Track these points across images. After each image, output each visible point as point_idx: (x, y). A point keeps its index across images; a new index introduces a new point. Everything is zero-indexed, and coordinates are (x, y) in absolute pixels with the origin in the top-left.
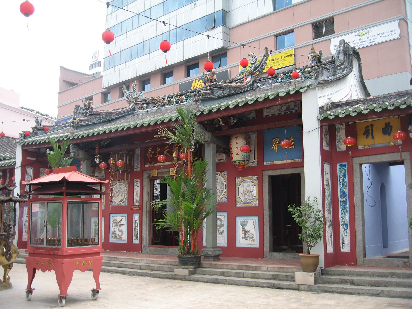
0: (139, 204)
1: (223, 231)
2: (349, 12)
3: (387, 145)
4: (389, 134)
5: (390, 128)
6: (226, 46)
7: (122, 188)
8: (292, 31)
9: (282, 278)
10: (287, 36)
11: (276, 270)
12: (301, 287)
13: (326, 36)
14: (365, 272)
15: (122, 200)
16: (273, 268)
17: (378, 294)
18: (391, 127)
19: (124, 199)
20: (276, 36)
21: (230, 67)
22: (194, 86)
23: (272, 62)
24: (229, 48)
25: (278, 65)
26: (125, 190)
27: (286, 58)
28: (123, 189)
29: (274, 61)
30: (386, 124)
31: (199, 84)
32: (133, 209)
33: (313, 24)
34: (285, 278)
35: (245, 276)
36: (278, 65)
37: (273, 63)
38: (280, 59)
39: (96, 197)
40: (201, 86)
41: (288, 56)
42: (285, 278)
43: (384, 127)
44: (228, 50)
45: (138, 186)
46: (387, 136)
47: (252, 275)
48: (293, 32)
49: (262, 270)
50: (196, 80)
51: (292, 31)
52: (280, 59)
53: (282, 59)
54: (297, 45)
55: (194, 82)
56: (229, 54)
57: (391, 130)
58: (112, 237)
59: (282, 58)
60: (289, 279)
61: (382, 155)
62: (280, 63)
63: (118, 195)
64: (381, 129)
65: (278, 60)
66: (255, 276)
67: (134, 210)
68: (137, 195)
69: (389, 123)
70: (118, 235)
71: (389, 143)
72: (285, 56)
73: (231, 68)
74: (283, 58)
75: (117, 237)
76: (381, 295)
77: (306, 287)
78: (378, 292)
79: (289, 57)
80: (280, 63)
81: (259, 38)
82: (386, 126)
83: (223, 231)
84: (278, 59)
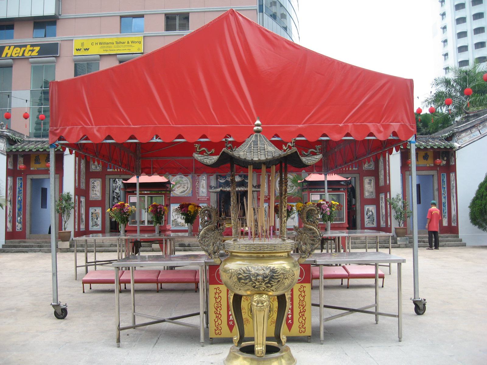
0: (206, 195)
1: (294, 217)
2: (206, 13)
3: (425, 165)
4: (427, 159)
5: (427, 156)
6: (57, 14)
7: (183, 181)
8: (142, 16)
9: (382, 243)
10: (135, 20)
11: (371, 239)
12: (401, 246)
13: (179, 30)
14: (425, 236)
15: (184, 191)
16: (369, 238)
17: (443, 246)
18: (428, 156)
19: (186, 190)
20: (121, 17)
21: (60, 39)
22: (7, 54)
23: (117, 45)
24: (60, 17)
25: (124, 50)
26: (187, 183)
27: (133, 44)
28: (185, 182)
29: (119, 45)
30: (425, 153)
31: (15, 51)
32: (200, 199)
33: (166, 14)
34: (384, 243)
35: (356, 243)
36: (124, 50)
37: (118, 47)
38: (126, 43)
39: (203, 187)
40: (17, 55)
41: (136, 42)
42: (384, 243)
43: (424, 155)
44: (59, 19)
45: (204, 180)
46: (425, 160)
47: (361, 242)
48: (144, 17)
49: (361, 239)
50: (10, 46)
51: (142, 16)
52: (126, 44)
53: (129, 44)
54: (147, 33)
55: (7, 48)
56: (59, 24)
57: (428, 157)
58: (173, 225)
59: (128, 43)
60: (387, 242)
61: (423, 171)
62: (127, 48)
63: (179, 187)
64: (422, 156)
65: (123, 45)
66: (363, 243)
67: (201, 200)
68: (203, 187)
69: (427, 153)
70: (180, 223)
71: (427, 165)
72: (132, 42)
73: (61, 40)
74: (130, 44)
75: (179, 224)
76: (445, 246)
77: (404, 245)
78: (443, 245)
79: (138, 44)
80: (127, 48)
81: (101, 15)
82: (425, 155)
83: (294, 217)
84: (124, 43)
